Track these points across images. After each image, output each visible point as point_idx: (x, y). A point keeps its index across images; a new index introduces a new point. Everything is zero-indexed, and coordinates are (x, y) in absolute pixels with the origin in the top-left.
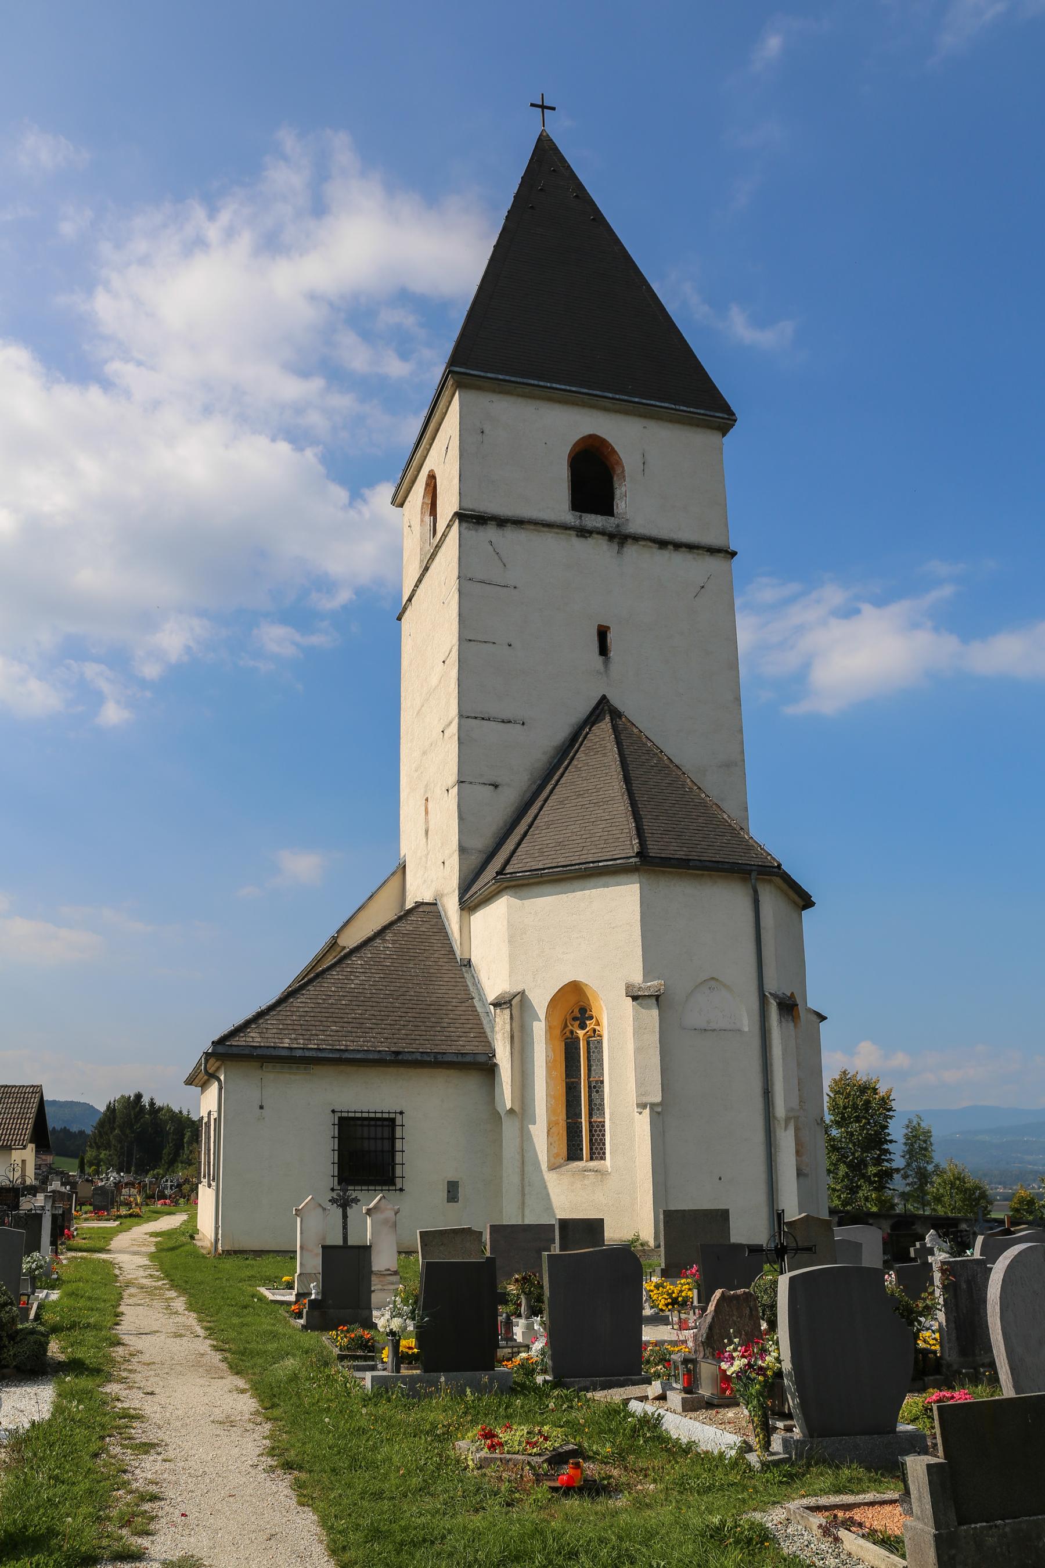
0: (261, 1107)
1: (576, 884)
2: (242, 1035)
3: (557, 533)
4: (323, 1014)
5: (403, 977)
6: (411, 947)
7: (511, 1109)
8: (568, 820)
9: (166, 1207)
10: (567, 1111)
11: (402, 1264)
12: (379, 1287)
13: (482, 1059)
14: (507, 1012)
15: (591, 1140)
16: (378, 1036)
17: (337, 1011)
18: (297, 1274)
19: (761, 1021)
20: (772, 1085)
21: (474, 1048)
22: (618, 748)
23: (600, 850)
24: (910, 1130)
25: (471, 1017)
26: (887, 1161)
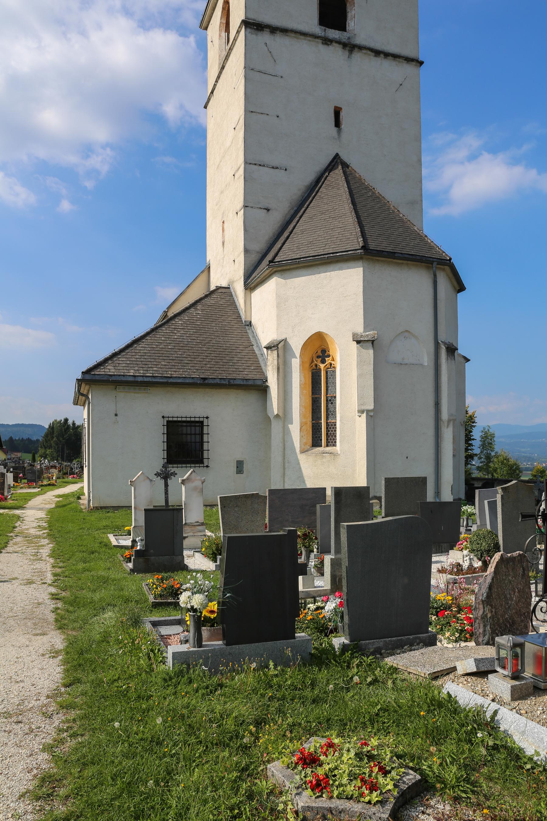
0: (116, 415)
1: (321, 268)
2: (102, 367)
3: (310, 41)
4: (156, 355)
5: (208, 332)
6: (213, 313)
7: (277, 414)
8: (316, 228)
9: (74, 479)
10: (312, 415)
11: (208, 513)
12: (191, 534)
13: (259, 383)
14: (275, 352)
15: (327, 434)
16: (192, 368)
17: (165, 352)
18: (132, 527)
19: (435, 359)
20: (440, 399)
21: (254, 376)
22: (347, 184)
23: (337, 246)
24: (483, 433)
25: (251, 357)
26: (470, 450)
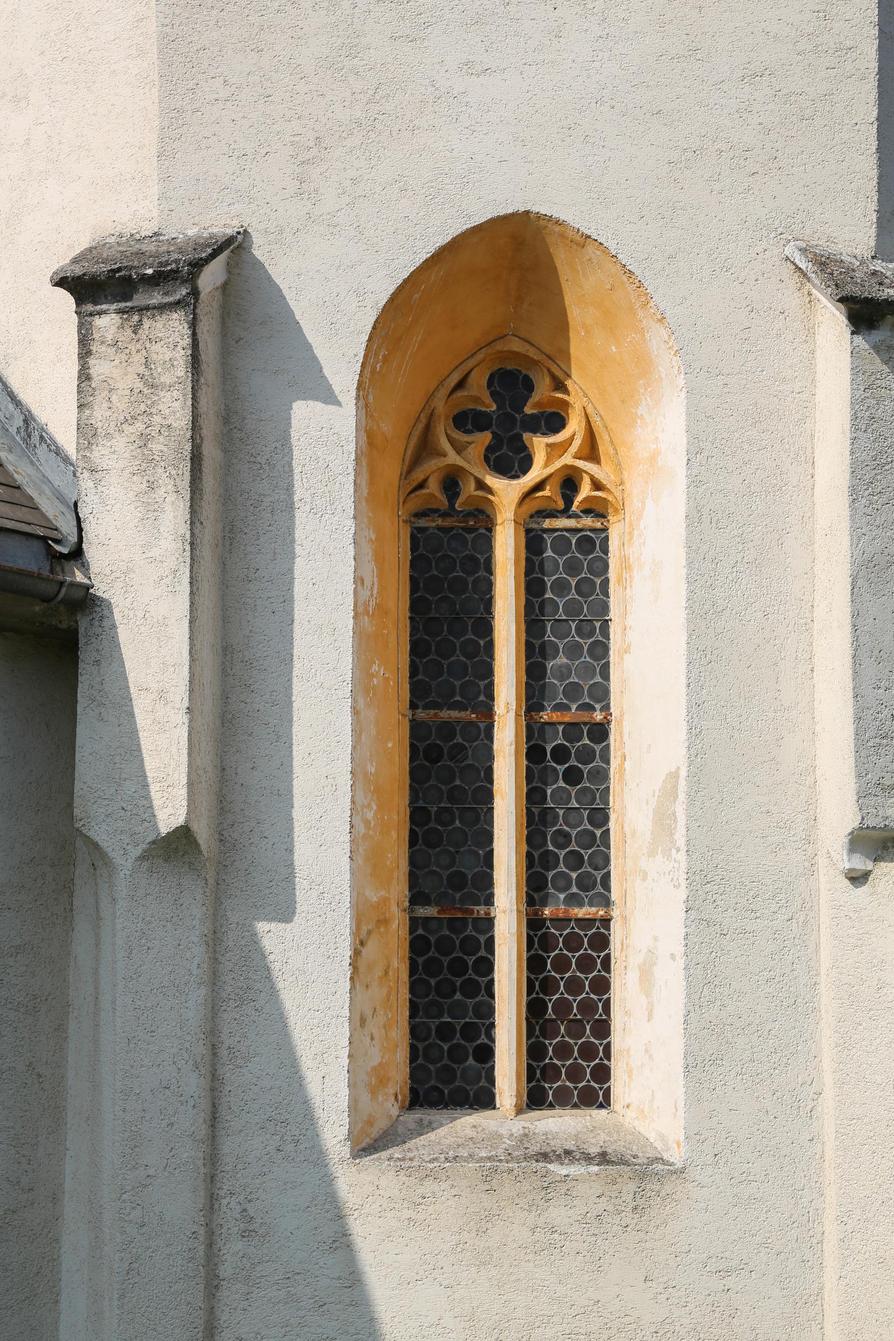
7: (184, 833)
10: (413, 862)
